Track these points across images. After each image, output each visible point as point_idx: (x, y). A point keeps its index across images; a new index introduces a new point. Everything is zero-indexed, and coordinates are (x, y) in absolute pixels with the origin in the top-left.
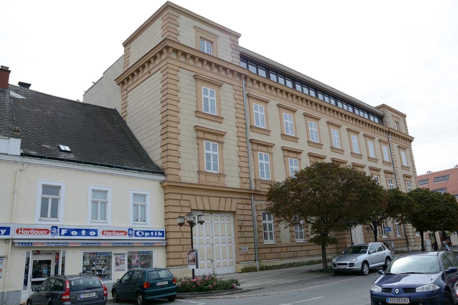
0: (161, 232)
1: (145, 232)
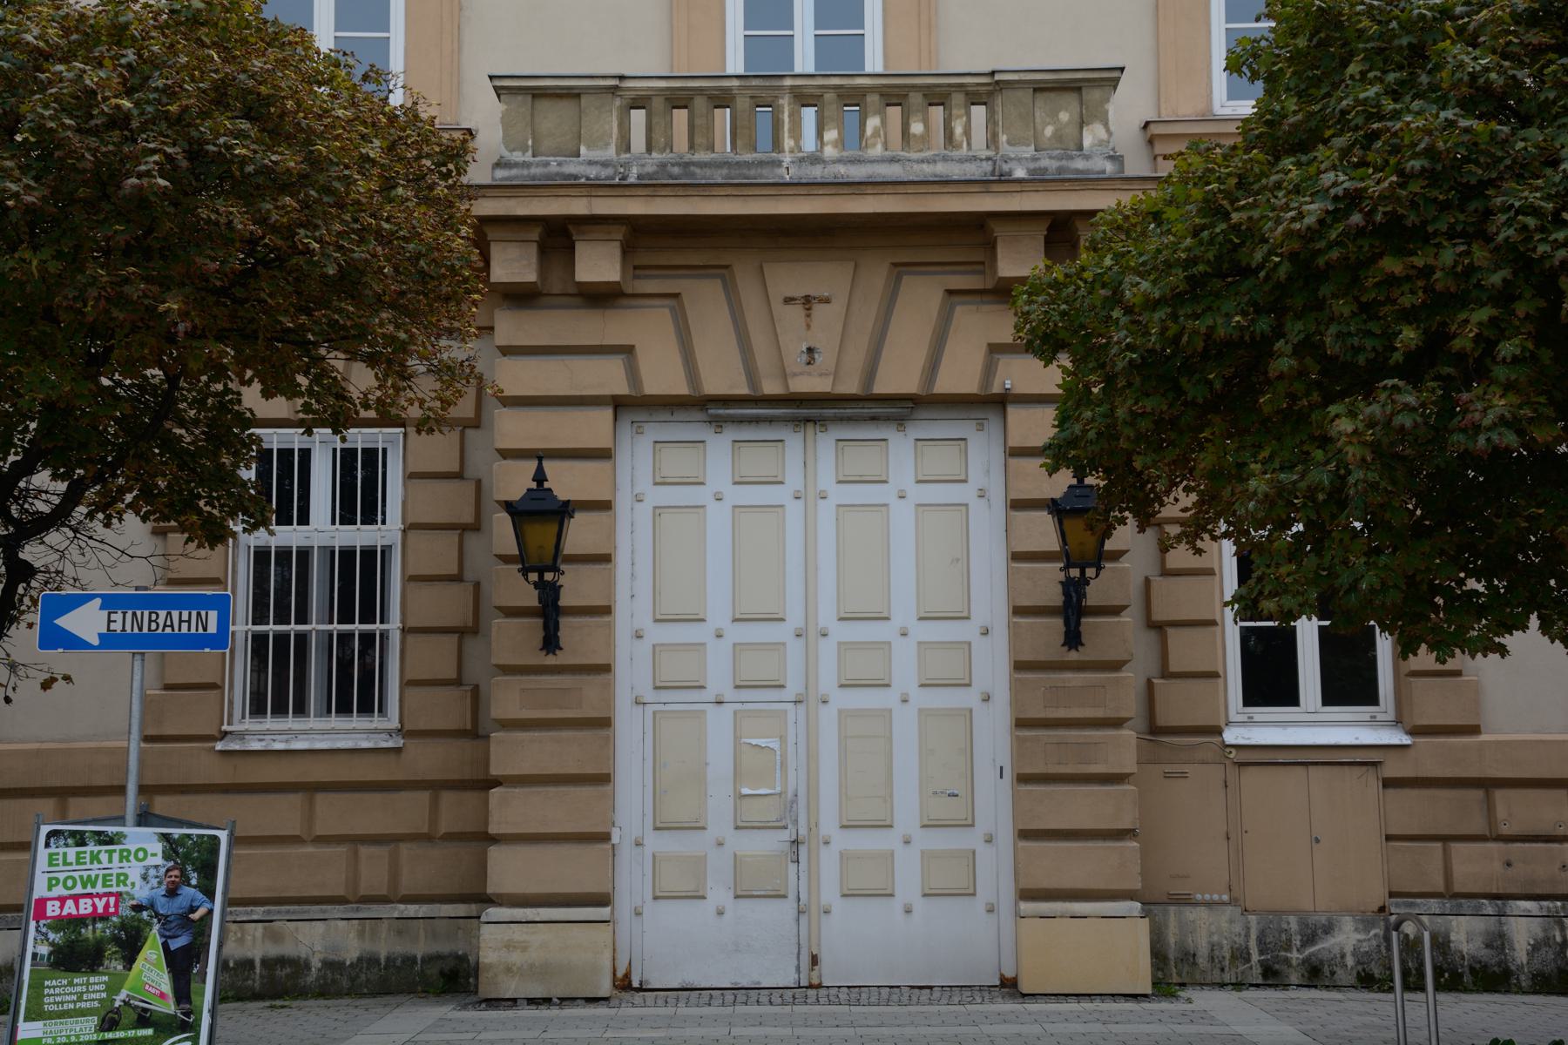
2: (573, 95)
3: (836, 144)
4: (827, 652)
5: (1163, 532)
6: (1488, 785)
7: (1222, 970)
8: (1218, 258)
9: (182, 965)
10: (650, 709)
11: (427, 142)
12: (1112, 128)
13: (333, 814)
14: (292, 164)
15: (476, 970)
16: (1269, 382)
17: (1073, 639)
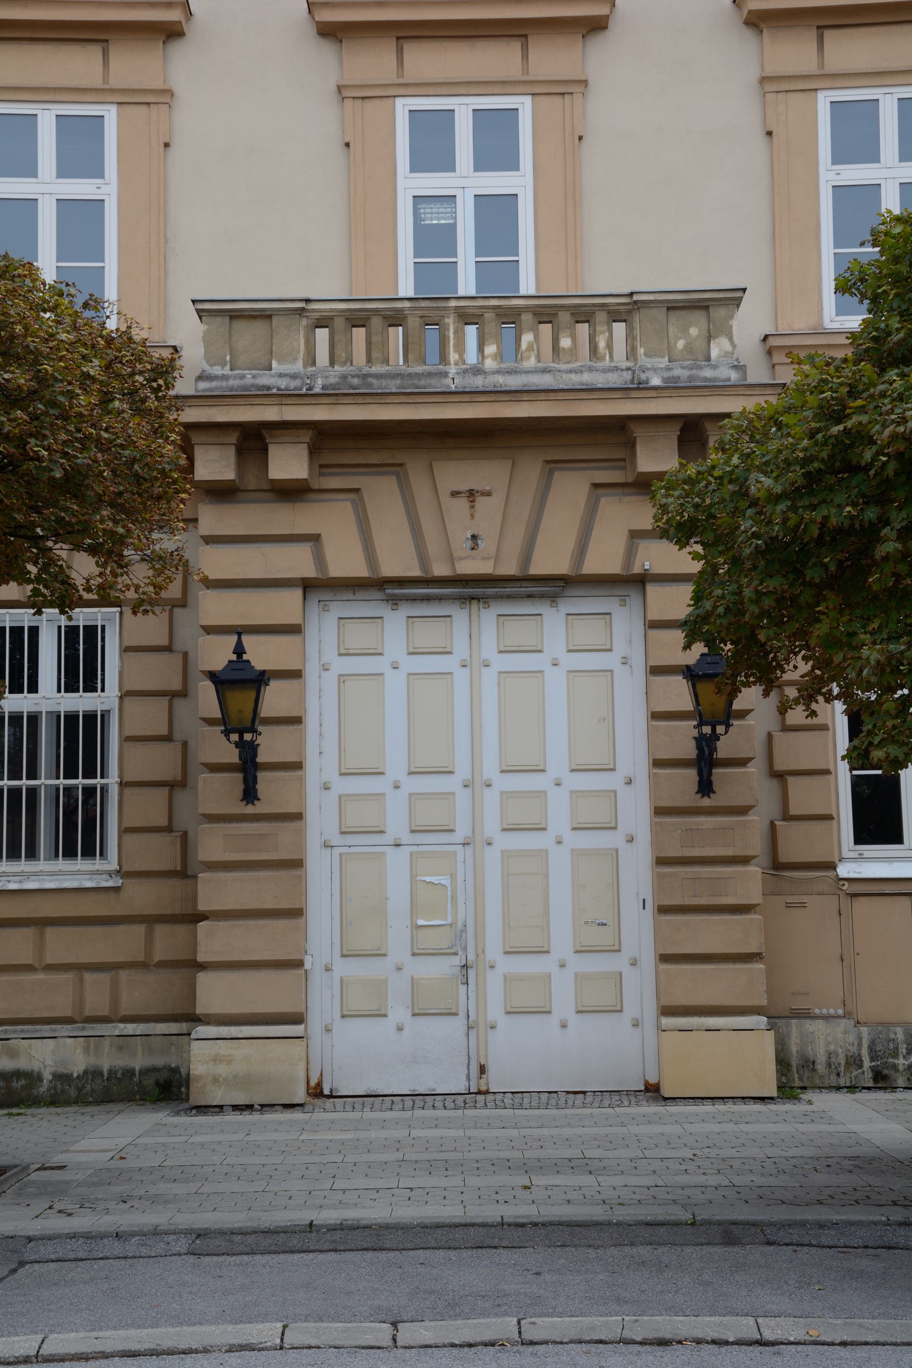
2: (265, 316)
3: (495, 357)
4: (491, 798)
5: (782, 694)
7: (838, 1075)
8: (832, 456)
10: (336, 852)
11: (140, 361)
12: (736, 341)
13: (62, 945)
14: (22, 381)
15: (187, 1081)
16: (875, 564)
17: (705, 787)
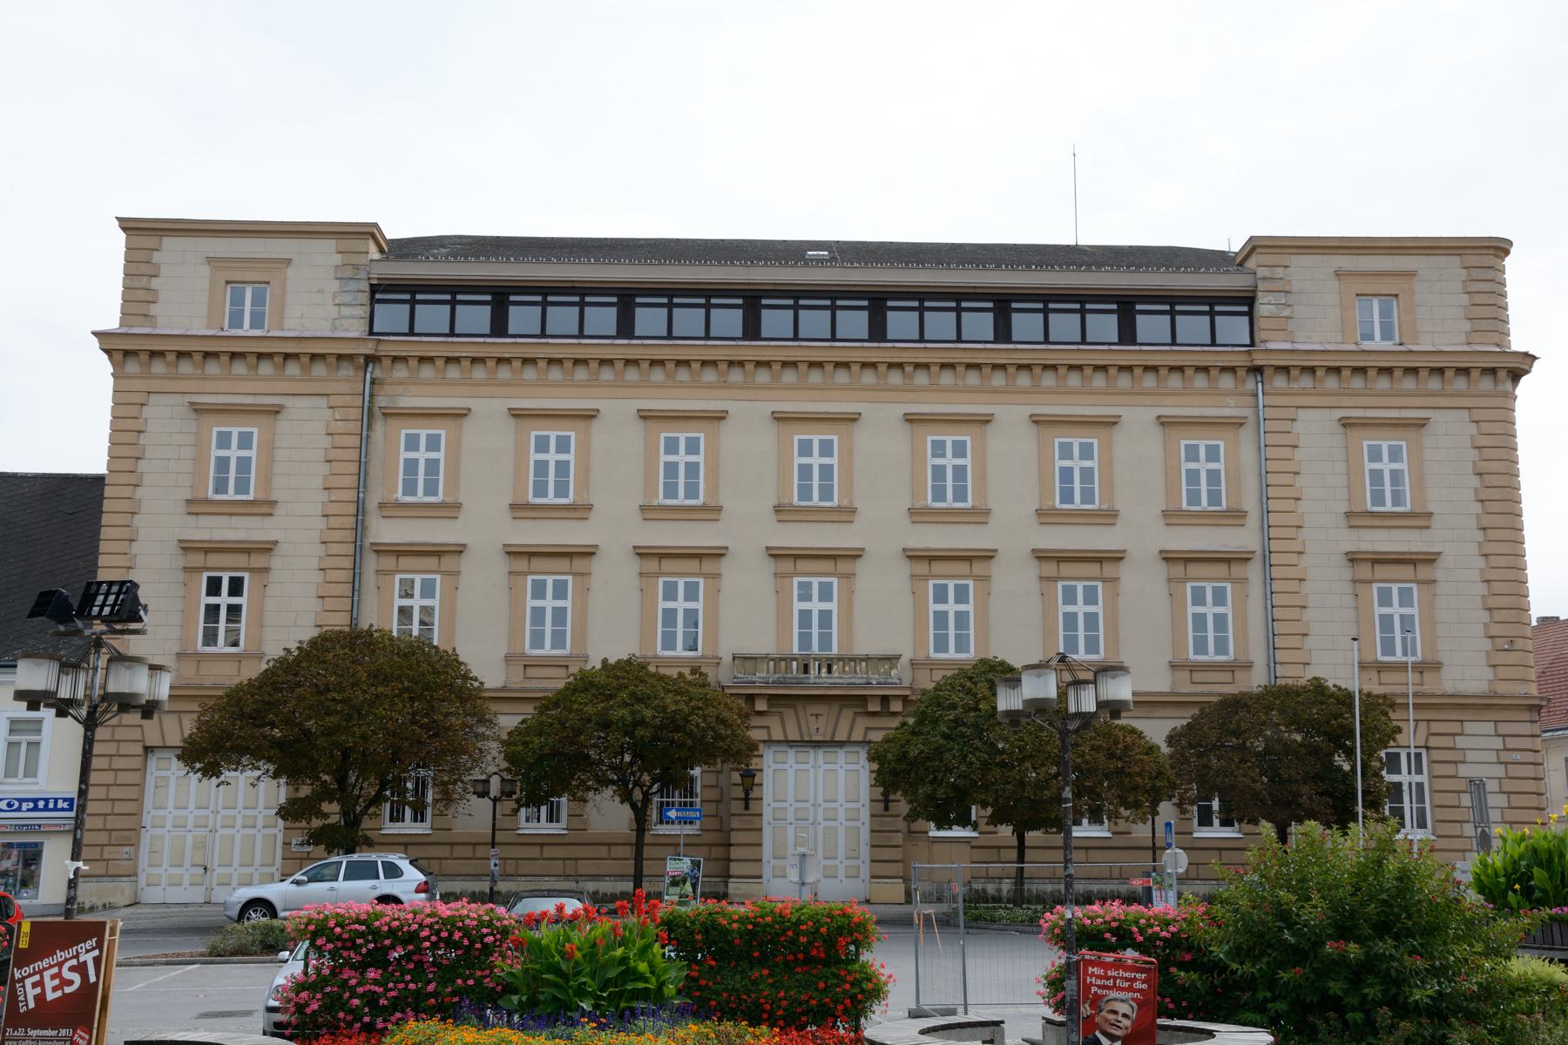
0: (65, 800)
1: (21, 801)
4: (820, 810)
6: (999, 848)
9: (694, 886)
17: (886, 809)
